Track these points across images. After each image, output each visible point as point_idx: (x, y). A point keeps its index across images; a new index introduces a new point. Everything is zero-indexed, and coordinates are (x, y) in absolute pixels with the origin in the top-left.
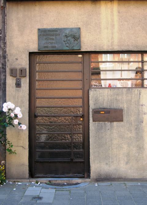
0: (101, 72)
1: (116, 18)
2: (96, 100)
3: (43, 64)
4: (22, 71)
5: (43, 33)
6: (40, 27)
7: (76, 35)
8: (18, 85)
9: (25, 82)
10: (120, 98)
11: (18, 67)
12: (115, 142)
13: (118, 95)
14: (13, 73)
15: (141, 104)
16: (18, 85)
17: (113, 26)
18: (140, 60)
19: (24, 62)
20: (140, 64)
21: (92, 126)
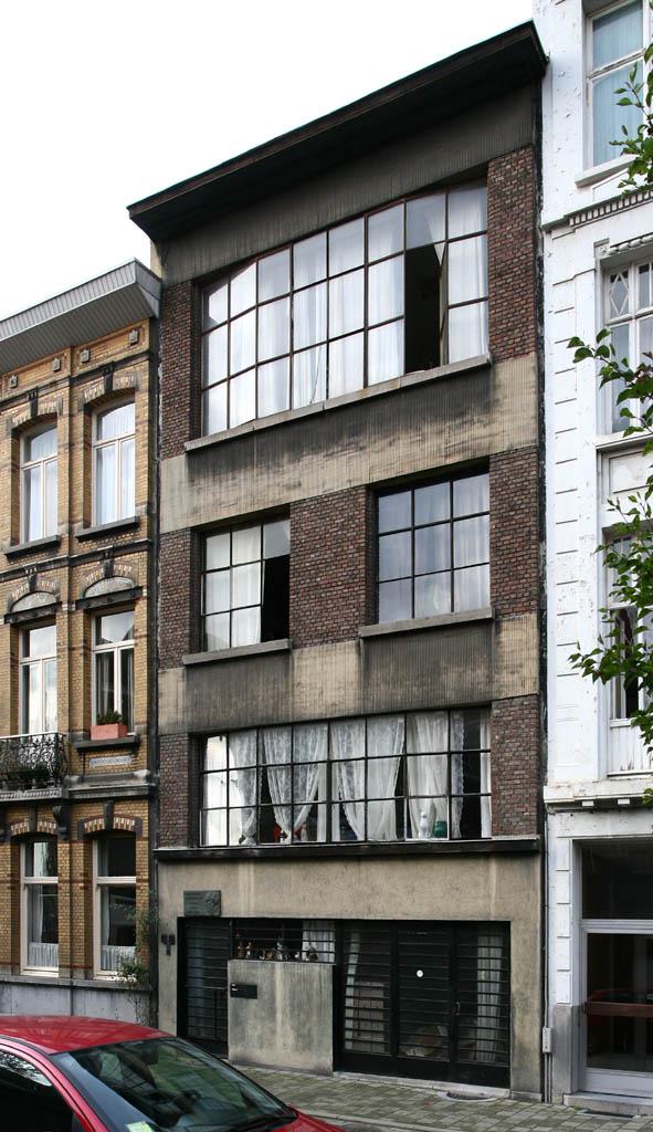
0: (393, 796)
1: (252, 879)
2: (234, 974)
3: (533, 722)
4: (172, 937)
5: (190, 897)
6: (186, 890)
7: (217, 899)
8: (169, 953)
9: (174, 949)
10: (254, 972)
11: (168, 934)
12: (251, 1022)
13: (253, 968)
14: (164, 937)
15: (588, 360)
16: (169, 953)
17: (250, 888)
18: (363, 803)
19: (173, 929)
20: (363, 797)
21: (231, 1000)
